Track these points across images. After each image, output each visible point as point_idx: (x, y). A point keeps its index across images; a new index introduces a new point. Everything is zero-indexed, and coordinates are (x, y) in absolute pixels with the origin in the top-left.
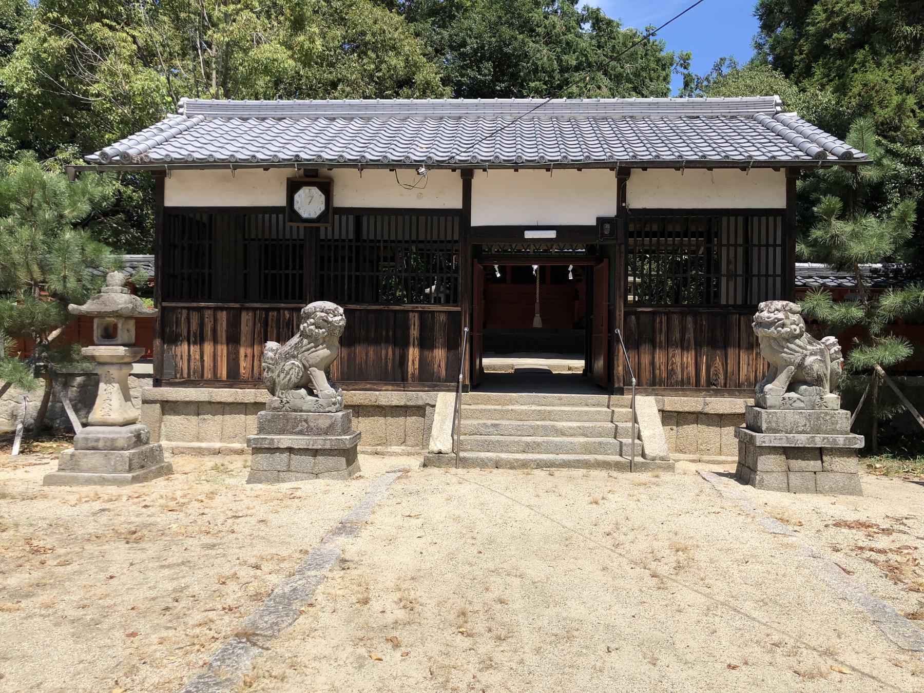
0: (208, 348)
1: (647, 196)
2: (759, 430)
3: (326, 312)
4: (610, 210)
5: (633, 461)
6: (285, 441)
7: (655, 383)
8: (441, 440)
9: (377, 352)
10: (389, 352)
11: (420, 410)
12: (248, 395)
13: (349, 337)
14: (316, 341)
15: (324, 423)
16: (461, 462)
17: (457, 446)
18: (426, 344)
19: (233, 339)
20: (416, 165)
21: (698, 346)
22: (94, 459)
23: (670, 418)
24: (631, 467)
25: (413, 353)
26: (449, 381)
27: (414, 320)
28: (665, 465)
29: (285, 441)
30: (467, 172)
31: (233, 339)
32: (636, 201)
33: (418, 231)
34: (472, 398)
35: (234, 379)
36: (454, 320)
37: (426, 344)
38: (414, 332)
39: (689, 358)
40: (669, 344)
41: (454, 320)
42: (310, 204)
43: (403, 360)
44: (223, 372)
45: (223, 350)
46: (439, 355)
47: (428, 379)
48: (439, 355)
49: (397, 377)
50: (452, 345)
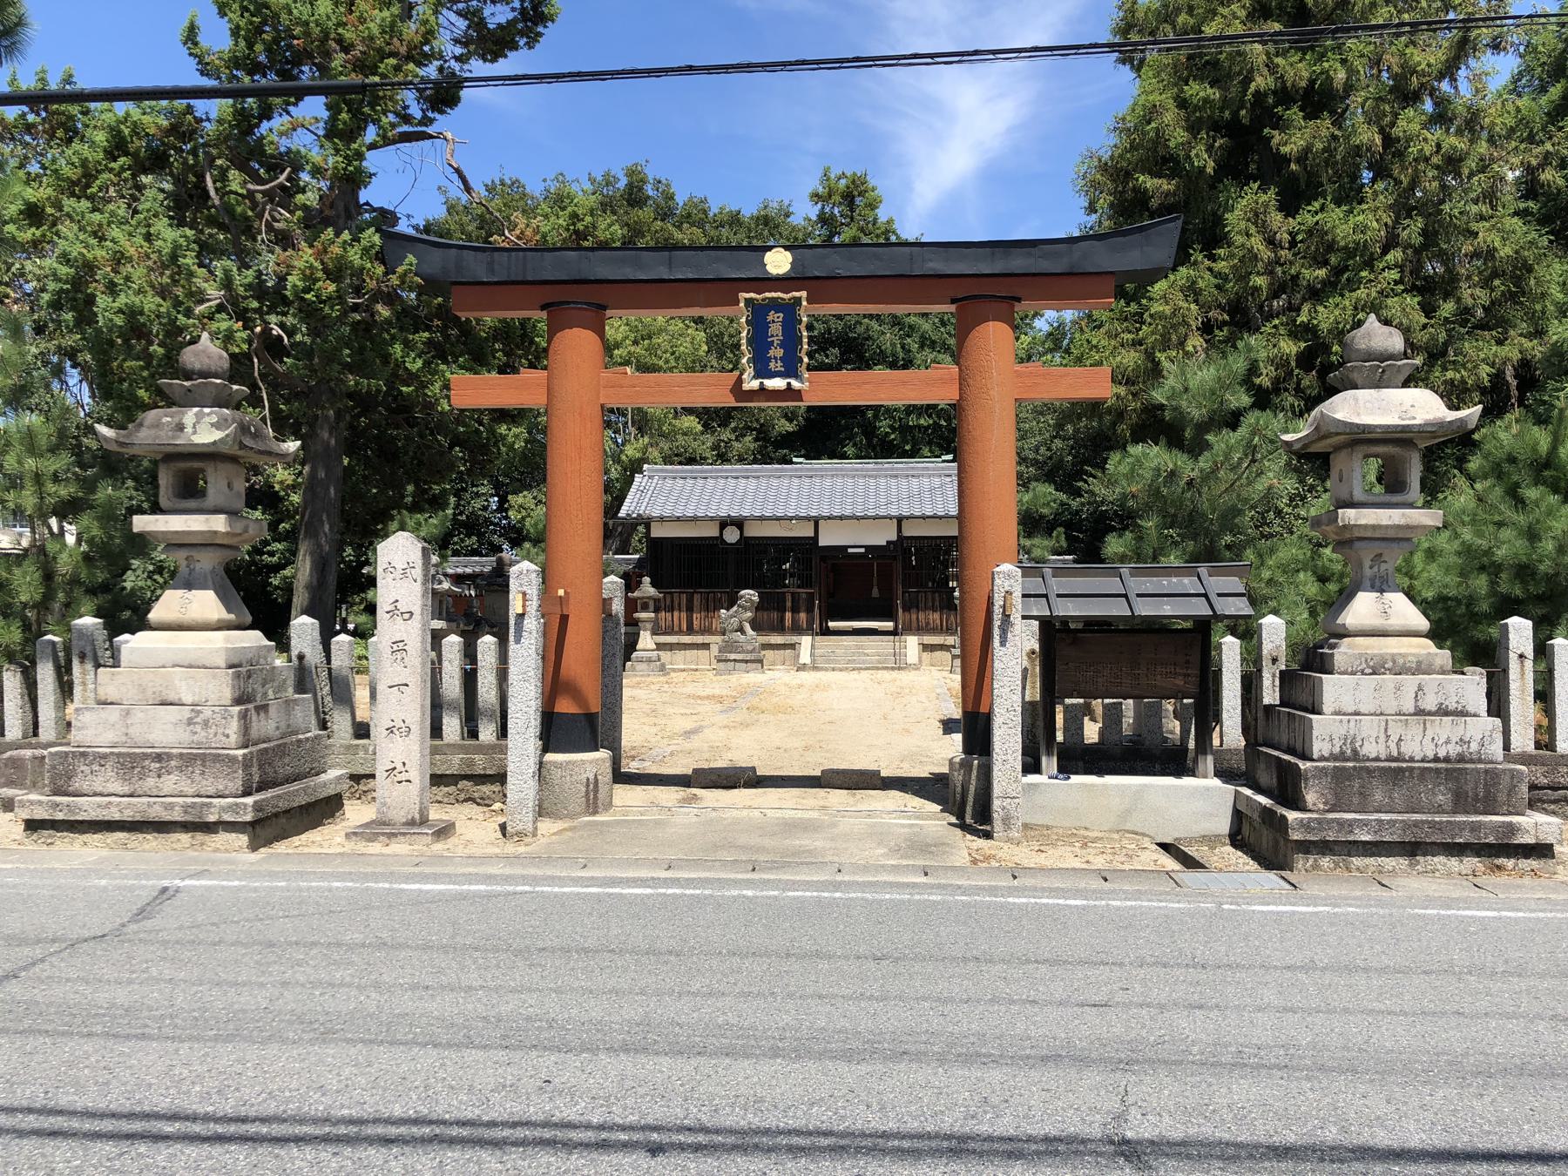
0: (676, 614)
1: (909, 531)
2: (1306, 757)
3: (750, 595)
4: (894, 537)
5: (900, 665)
6: (733, 656)
7: (919, 630)
8: (805, 657)
9: (770, 618)
10: (775, 615)
11: (792, 646)
12: (699, 639)
13: (759, 608)
14: (745, 609)
15: (750, 648)
16: (815, 668)
17: (813, 661)
18: (795, 610)
19: (690, 609)
20: (791, 519)
21: (941, 609)
22: (643, 666)
23: (926, 648)
24: (899, 669)
25: (788, 615)
26: (809, 630)
27: (789, 597)
28: (916, 667)
29: (733, 656)
30: (816, 521)
31: (690, 609)
32: (907, 533)
33: (801, 1049)
34: (906, 765)
35: (690, 631)
36: (811, 597)
37: (795, 610)
38: (789, 604)
39: (937, 616)
40: (926, 608)
41: (811, 597)
42: (731, 536)
43: (782, 619)
44: (684, 627)
45: (684, 615)
46: (803, 616)
47: (797, 629)
48: (803, 616)
49: (780, 628)
50: (810, 610)
